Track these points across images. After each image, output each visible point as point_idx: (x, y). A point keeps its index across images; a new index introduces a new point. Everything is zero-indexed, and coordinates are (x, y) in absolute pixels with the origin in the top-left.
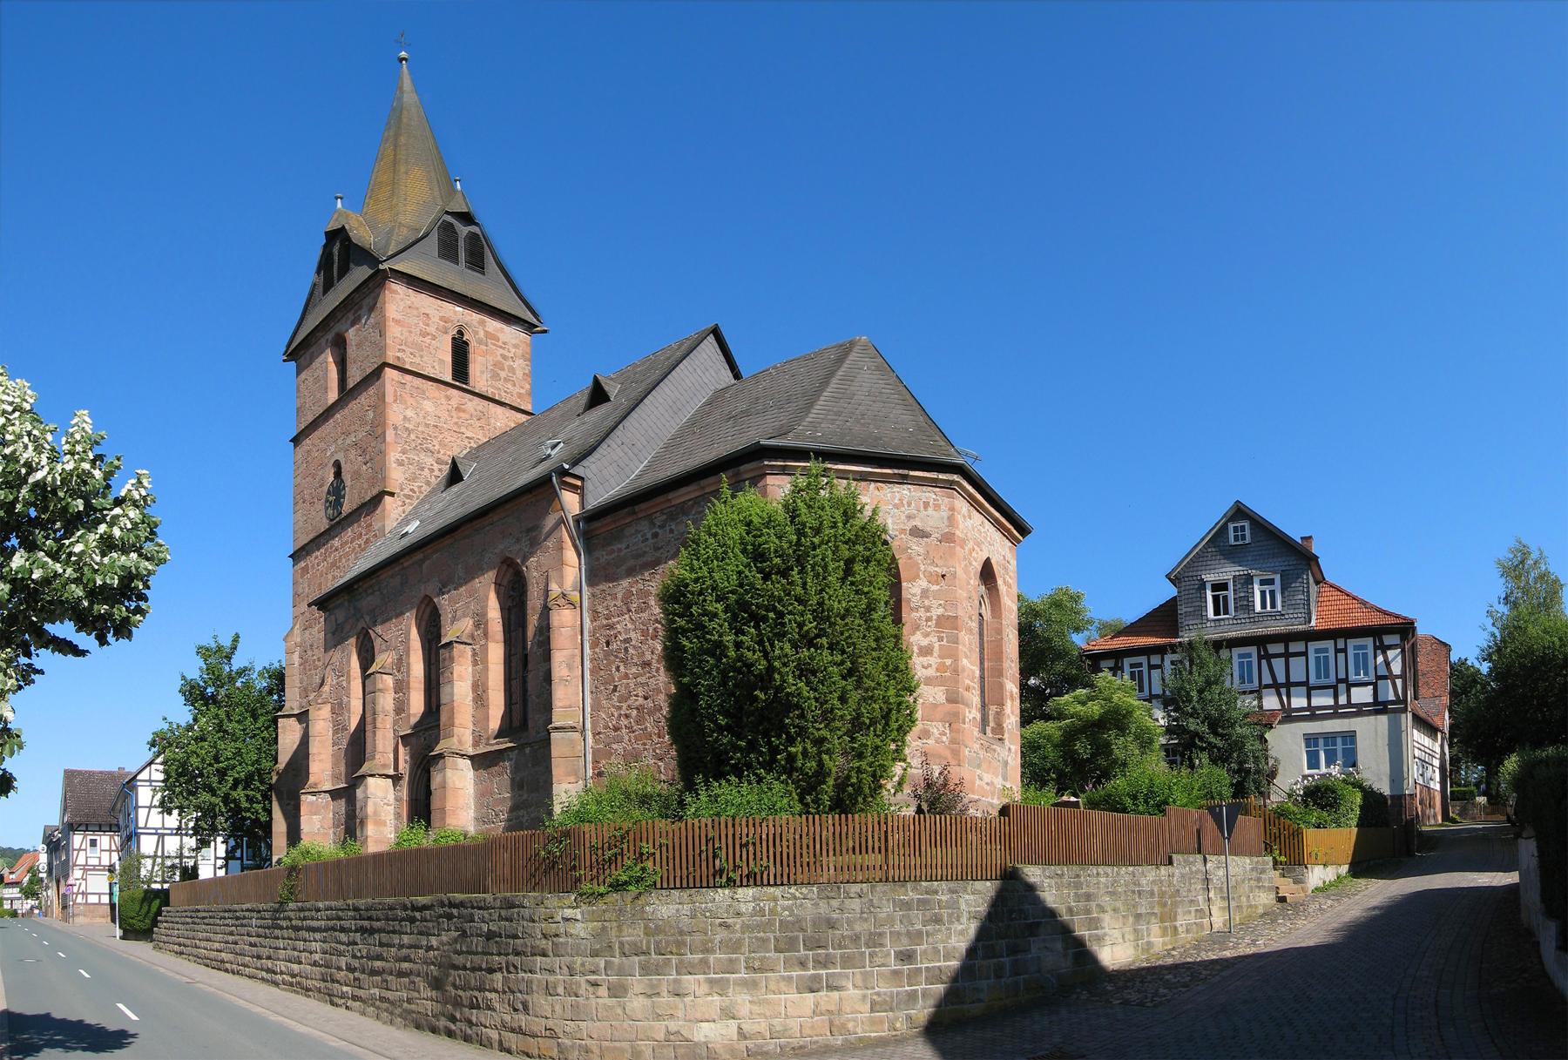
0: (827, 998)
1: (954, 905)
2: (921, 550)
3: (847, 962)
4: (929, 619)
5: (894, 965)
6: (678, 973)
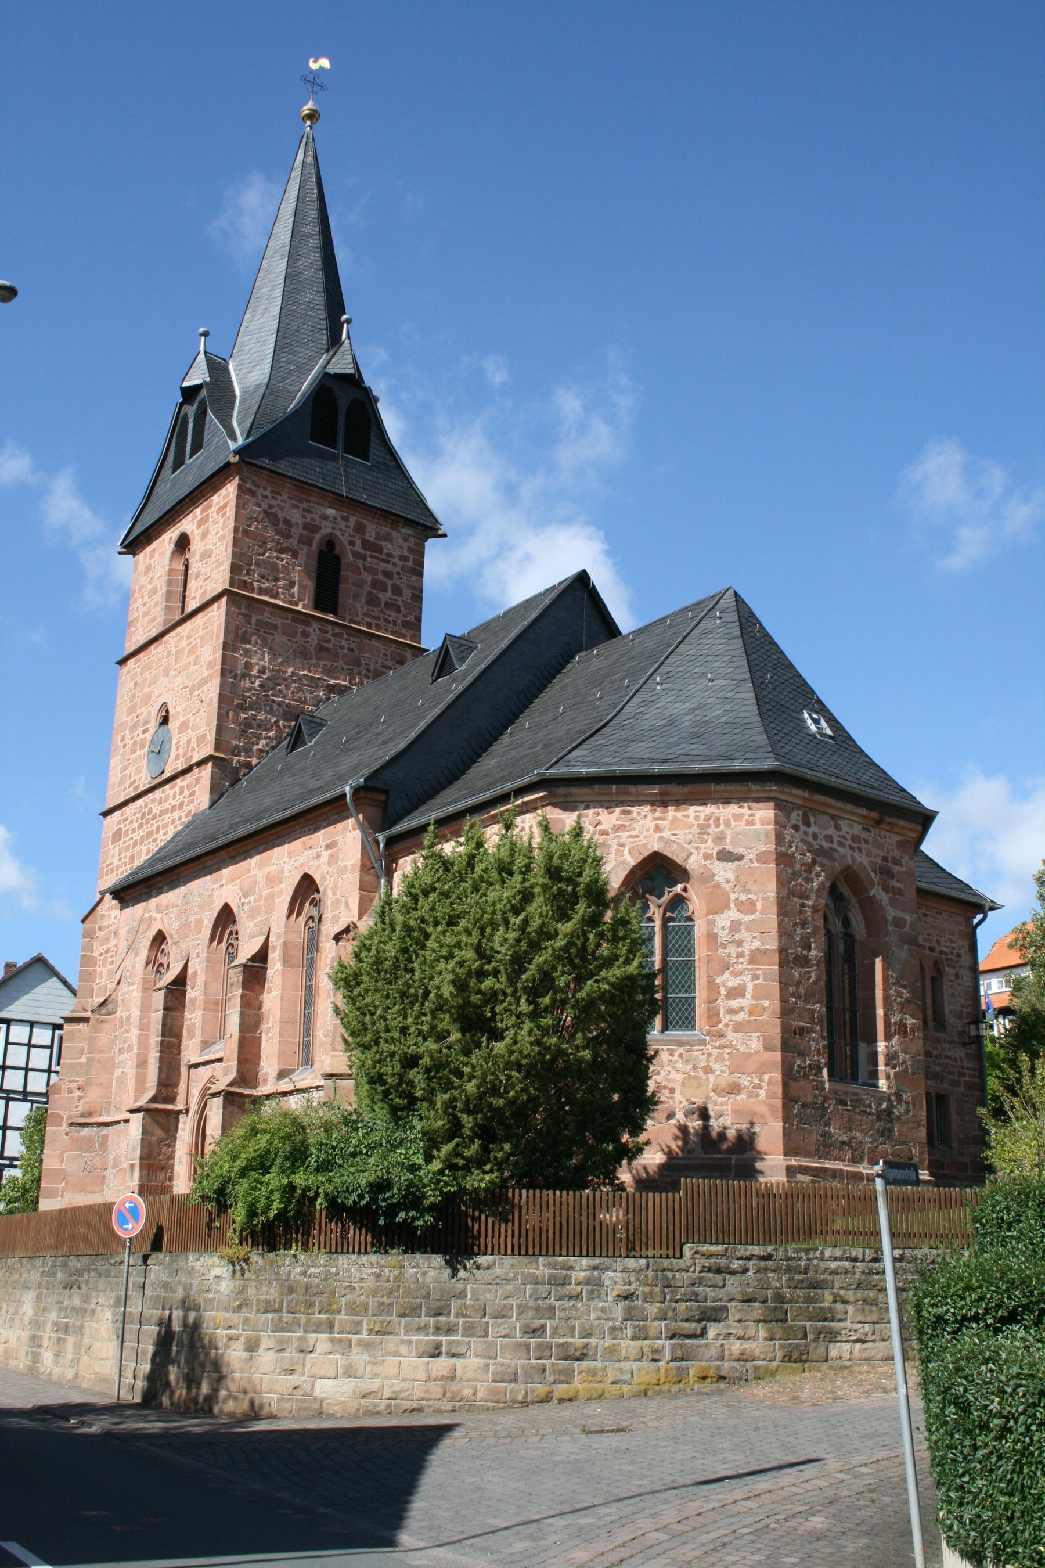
0: (441, 1366)
1: (595, 1285)
2: (731, 876)
3: (469, 1330)
4: (740, 955)
5: (519, 1338)
6: (305, 1332)
